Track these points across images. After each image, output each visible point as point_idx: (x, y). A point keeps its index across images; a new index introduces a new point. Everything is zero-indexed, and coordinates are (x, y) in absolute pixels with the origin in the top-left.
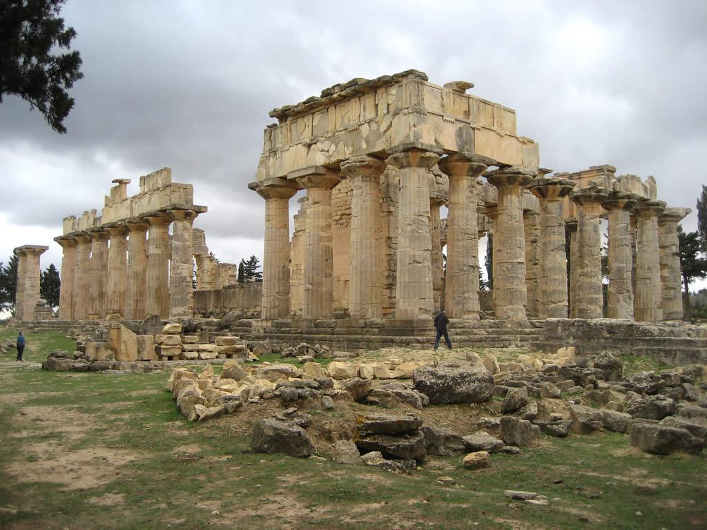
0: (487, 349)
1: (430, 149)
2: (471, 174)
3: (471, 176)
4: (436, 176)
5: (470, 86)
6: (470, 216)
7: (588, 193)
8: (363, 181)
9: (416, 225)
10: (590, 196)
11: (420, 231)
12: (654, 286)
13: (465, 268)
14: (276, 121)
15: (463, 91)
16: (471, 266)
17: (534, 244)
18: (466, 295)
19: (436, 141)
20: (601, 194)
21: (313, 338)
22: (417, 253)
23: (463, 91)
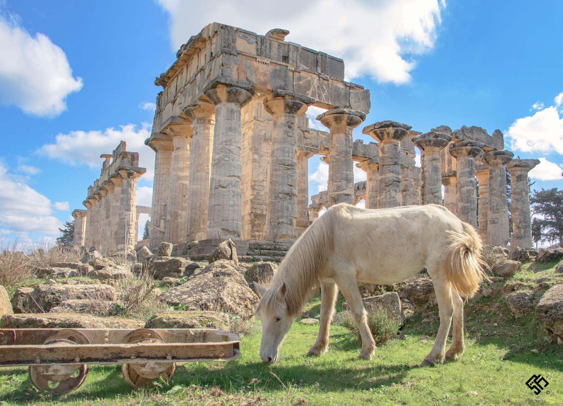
0: (179, 232)
1: (236, 84)
2: (288, 111)
3: (289, 113)
4: (303, 132)
5: (285, 33)
6: (286, 149)
7: (427, 138)
8: (198, 123)
9: (223, 153)
10: (430, 141)
11: (227, 159)
12: (502, 225)
13: (281, 196)
14: (161, 89)
15: (281, 38)
16: (287, 194)
17: (404, 193)
18: (280, 220)
19: (247, 79)
20: (439, 139)
21: (370, 327)
22: (223, 179)
23: (281, 38)
